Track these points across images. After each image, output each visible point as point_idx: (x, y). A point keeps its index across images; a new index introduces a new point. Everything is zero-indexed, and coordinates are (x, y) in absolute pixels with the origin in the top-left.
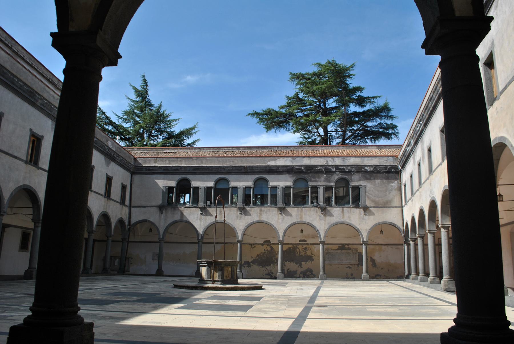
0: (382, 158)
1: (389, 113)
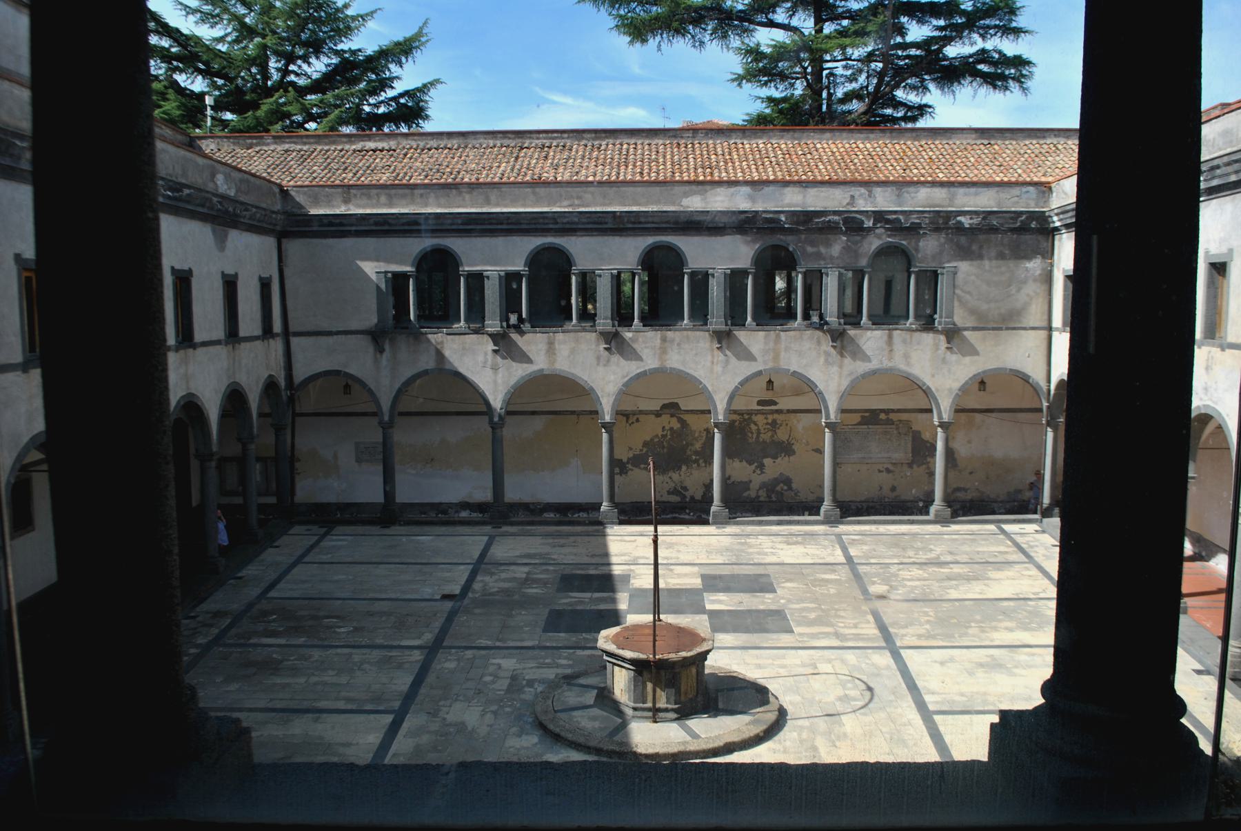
1: (1011, 21)
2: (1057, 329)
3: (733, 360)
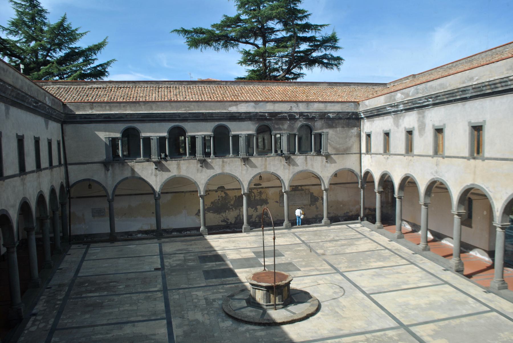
0: (344, 104)
1: (335, 44)
2: (364, 154)
3: (250, 169)
